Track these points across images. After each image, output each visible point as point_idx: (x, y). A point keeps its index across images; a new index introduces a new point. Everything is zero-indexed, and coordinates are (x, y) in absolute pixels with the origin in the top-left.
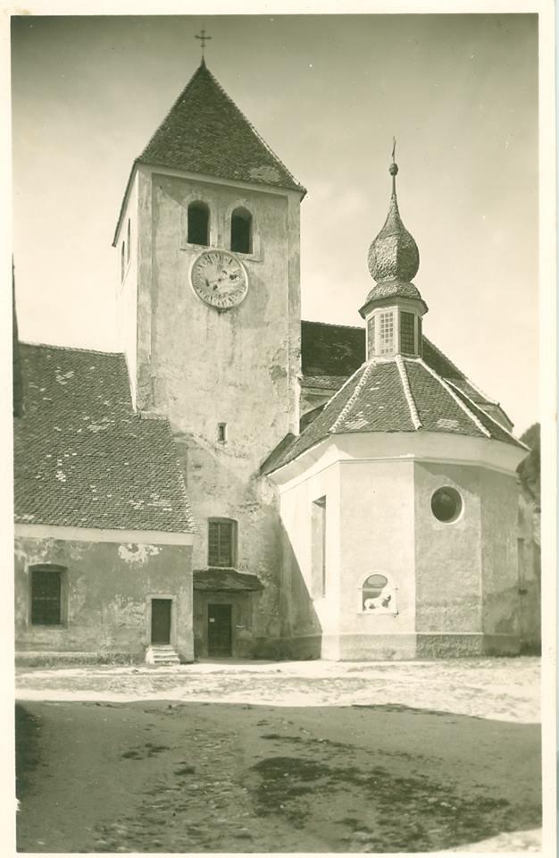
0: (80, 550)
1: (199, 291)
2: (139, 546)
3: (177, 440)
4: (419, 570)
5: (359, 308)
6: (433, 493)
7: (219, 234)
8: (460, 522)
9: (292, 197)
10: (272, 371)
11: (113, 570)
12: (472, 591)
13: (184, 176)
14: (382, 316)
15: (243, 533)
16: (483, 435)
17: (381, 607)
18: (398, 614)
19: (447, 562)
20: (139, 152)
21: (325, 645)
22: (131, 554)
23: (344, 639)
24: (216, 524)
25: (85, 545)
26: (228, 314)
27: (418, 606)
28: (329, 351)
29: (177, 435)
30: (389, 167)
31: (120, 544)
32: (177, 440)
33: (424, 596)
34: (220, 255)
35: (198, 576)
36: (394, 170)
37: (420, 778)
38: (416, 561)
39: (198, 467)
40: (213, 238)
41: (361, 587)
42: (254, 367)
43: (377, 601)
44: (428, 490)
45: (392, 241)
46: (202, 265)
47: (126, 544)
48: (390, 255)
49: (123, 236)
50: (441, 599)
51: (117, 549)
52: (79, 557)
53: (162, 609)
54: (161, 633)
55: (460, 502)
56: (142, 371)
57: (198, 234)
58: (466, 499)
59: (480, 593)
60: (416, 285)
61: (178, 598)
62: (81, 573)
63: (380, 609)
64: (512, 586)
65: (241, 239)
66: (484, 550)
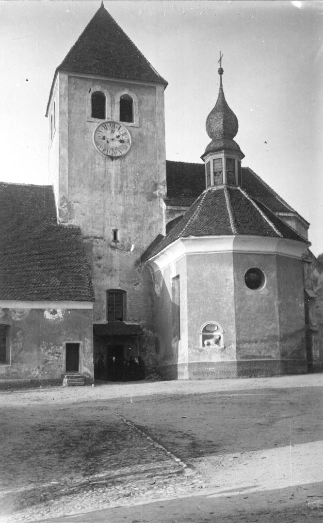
0: (19, 314)
1: (99, 147)
2: (57, 311)
3: (85, 241)
4: (237, 320)
5: (201, 156)
6: (246, 272)
7: (113, 111)
8: (263, 289)
9: (159, 88)
10: (147, 195)
11: (41, 326)
12: (272, 333)
13: (85, 76)
14: (214, 160)
15: (130, 299)
16: (277, 236)
17: (214, 344)
18: (225, 348)
19: (256, 314)
20: (59, 62)
21: (180, 370)
22: (52, 316)
23: (191, 365)
24: (112, 294)
25: (22, 312)
26: (118, 161)
27: (238, 343)
28: (183, 181)
29: (86, 238)
30: (217, 70)
31: (45, 310)
32: (85, 241)
33: (241, 337)
34: (113, 123)
35: (97, 329)
36: (221, 71)
37: (36, 402)
38: (236, 315)
39: (100, 258)
40: (108, 114)
41: (201, 332)
42: (135, 193)
43: (212, 341)
44: (243, 270)
45: (220, 115)
46: (101, 130)
47: (49, 309)
48: (219, 125)
49: (51, 112)
50: (253, 338)
51: (43, 314)
52: (18, 319)
53: (73, 351)
54: (72, 363)
55: (264, 277)
56: (63, 199)
57: (98, 110)
58: (267, 275)
59: (278, 334)
60: (237, 142)
61: (84, 343)
62: (19, 329)
63: (214, 346)
64: (301, 328)
65: (126, 114)
66: (280, 306)
